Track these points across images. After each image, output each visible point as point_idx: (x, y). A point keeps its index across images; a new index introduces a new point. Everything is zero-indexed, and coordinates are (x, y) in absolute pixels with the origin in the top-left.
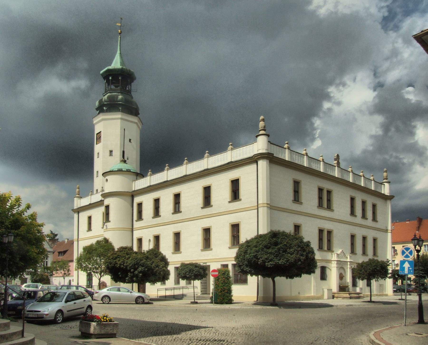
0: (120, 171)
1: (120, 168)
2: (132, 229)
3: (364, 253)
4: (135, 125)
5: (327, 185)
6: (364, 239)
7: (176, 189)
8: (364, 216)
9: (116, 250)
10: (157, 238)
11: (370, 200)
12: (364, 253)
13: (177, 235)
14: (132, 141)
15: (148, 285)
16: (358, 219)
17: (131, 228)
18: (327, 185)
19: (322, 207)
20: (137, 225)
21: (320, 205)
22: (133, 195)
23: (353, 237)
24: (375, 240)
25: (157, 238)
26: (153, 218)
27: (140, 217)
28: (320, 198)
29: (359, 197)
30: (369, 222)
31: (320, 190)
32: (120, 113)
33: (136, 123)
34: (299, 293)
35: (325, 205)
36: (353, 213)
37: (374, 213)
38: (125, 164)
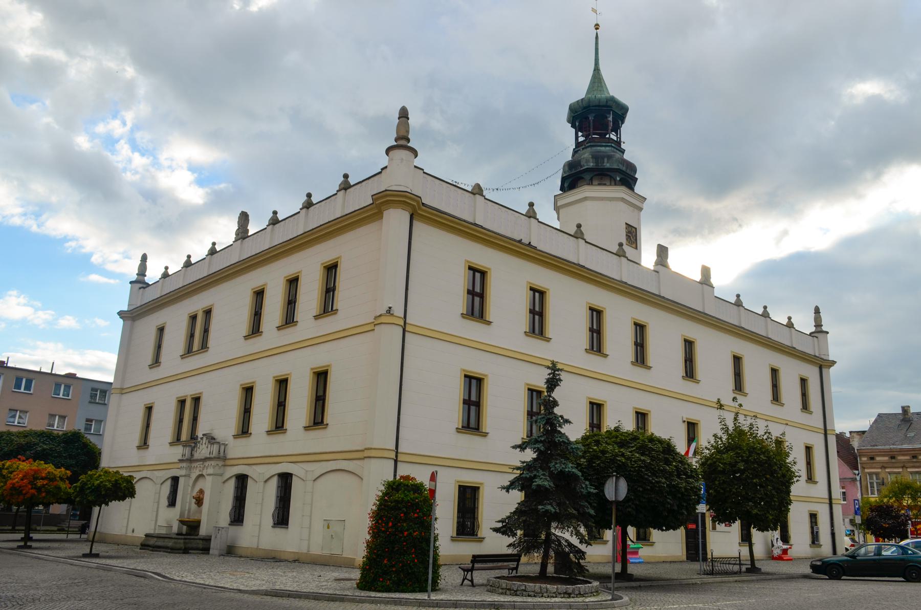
4: (622, 204)
13: (321, 377)
26: (246, 338)
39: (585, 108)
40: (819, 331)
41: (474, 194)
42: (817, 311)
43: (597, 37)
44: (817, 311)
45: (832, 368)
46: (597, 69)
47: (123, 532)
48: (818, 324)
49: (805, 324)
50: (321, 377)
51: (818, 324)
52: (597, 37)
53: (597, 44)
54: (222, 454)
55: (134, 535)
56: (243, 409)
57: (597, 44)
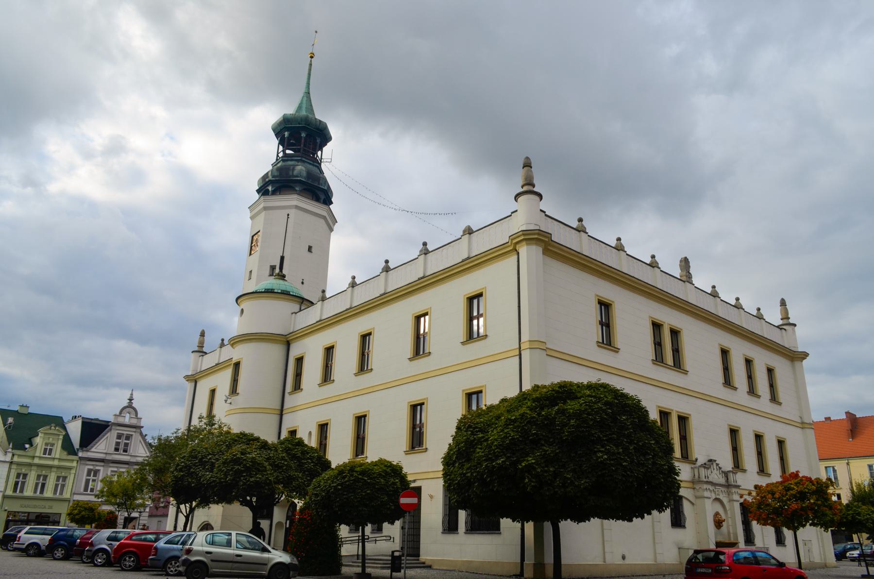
0: (269, 292)
1: (269, 287)
2: (282, 410)
3: (762, 470)
4: (322, 221)
5: (670, 318)
6: (759, 438)
7: (361, 324)
8: (752, 391)
9: (668, 511)
10: (323, 428)
11: (762, 359)
12: (762, 470)
13: (360, 420)
14: (313, 250)
15: (386, 525)
16: (741, 395)
17: (279, 407)
18: (670, 318)
19: (662, 362)
20: (290, 401)
21: (659, 359)
22: (287, 342)
23: (734, 433)
24: (781, 443)
25: (323, 428)
26: (320, 385)
27: (297, 387)
28: (658, 344)
29: (739, 350)
30: (764, 403)
31: (657, 327)
32: (296, 196)
33: (324, 218)
34: (624, 558)
35: (669, 359)
36: (728, 382)
37: (772, 386)
38: (281, 282)
39: (318, 129)
40: (787, 324)
41: (579, 231)
42: (783, 303)
43: (311, 65)
44: (783, 303)
45: (804, 361)
46: (308, 93)
47: (599, 561)
48: (786, 317)
49: (774, 316)
50: (360, 420)
51: (786, 317)
52: (311, 65)
53: (310, 70)
54: (697, 477)
55: (627, 562)
56: (688, 437)
57: (310, 70)
